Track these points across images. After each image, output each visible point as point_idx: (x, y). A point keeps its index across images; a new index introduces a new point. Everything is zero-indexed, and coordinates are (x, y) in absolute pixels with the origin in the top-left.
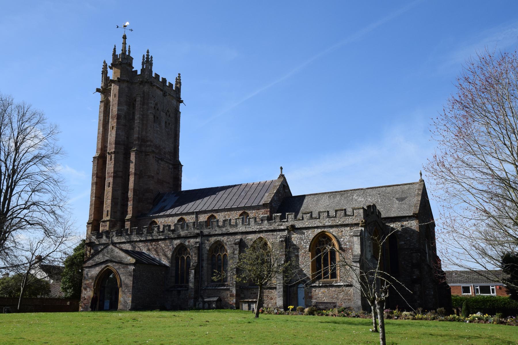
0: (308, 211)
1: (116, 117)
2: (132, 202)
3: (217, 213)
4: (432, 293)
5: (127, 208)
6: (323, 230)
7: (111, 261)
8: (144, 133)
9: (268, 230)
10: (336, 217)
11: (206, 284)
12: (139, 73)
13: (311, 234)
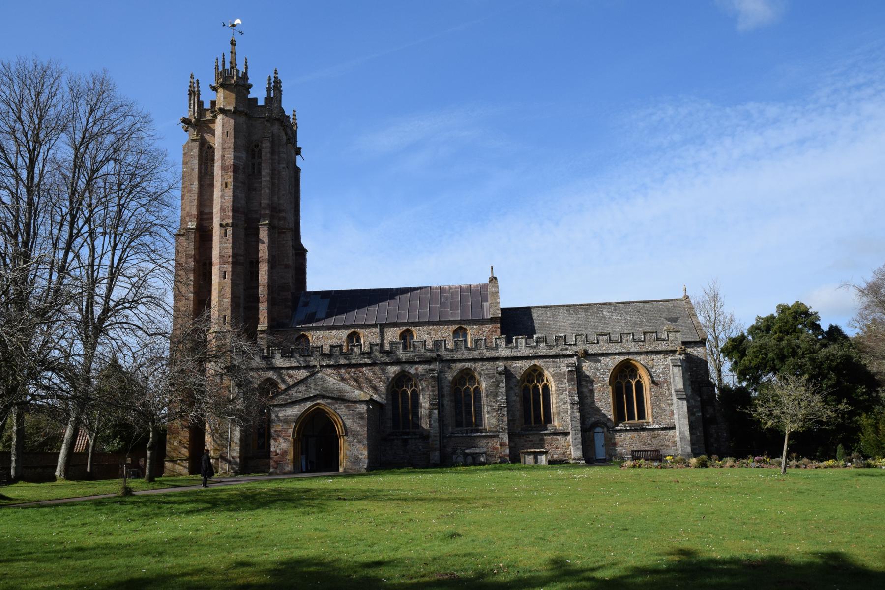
0: (605, 332)
1: (232, 168)
2: (266, 304)
3: (416, 327)
4: (725, 435)
5: (258, 314)
6: (627, 357)
7: (323, 397)
8: (276, 198)
9: (547, 356)
10: (644, 341)
11: (450, 429)
12: (261, 102)
13: (612, 363)
